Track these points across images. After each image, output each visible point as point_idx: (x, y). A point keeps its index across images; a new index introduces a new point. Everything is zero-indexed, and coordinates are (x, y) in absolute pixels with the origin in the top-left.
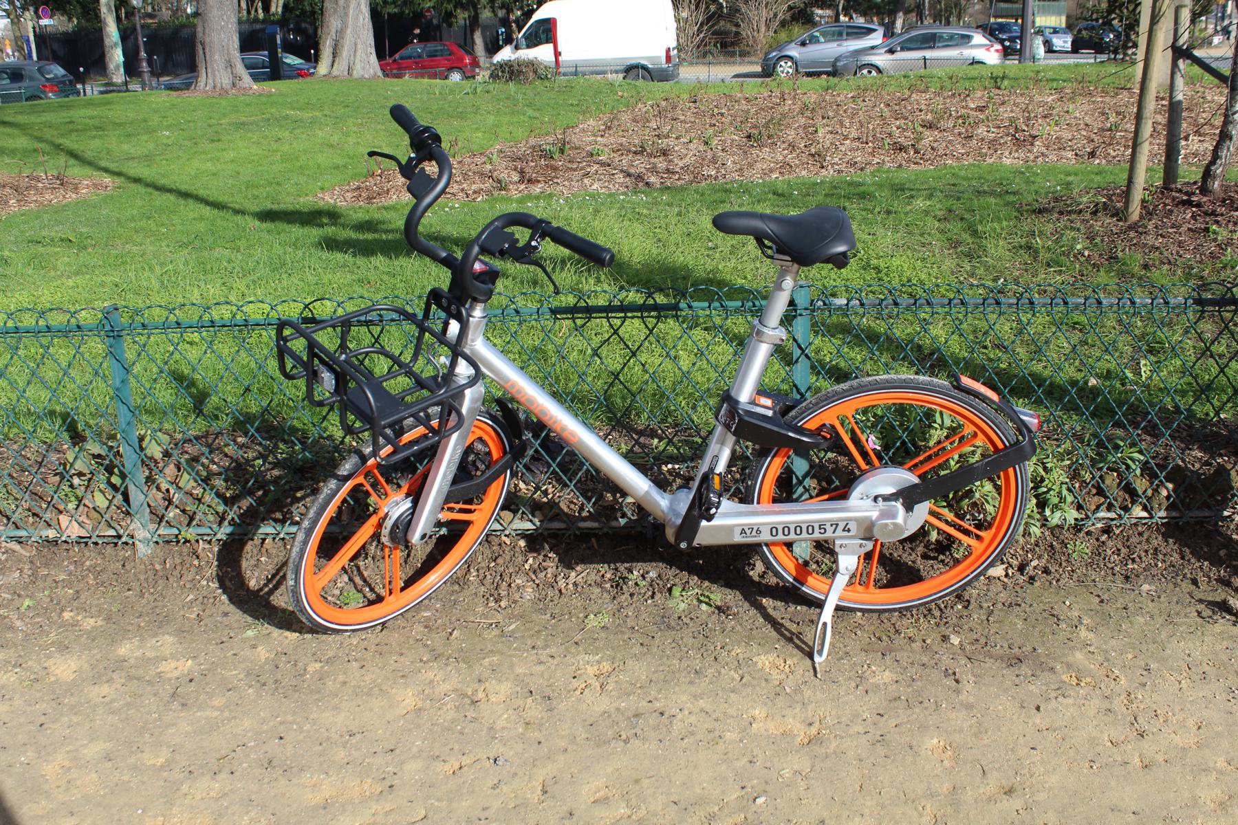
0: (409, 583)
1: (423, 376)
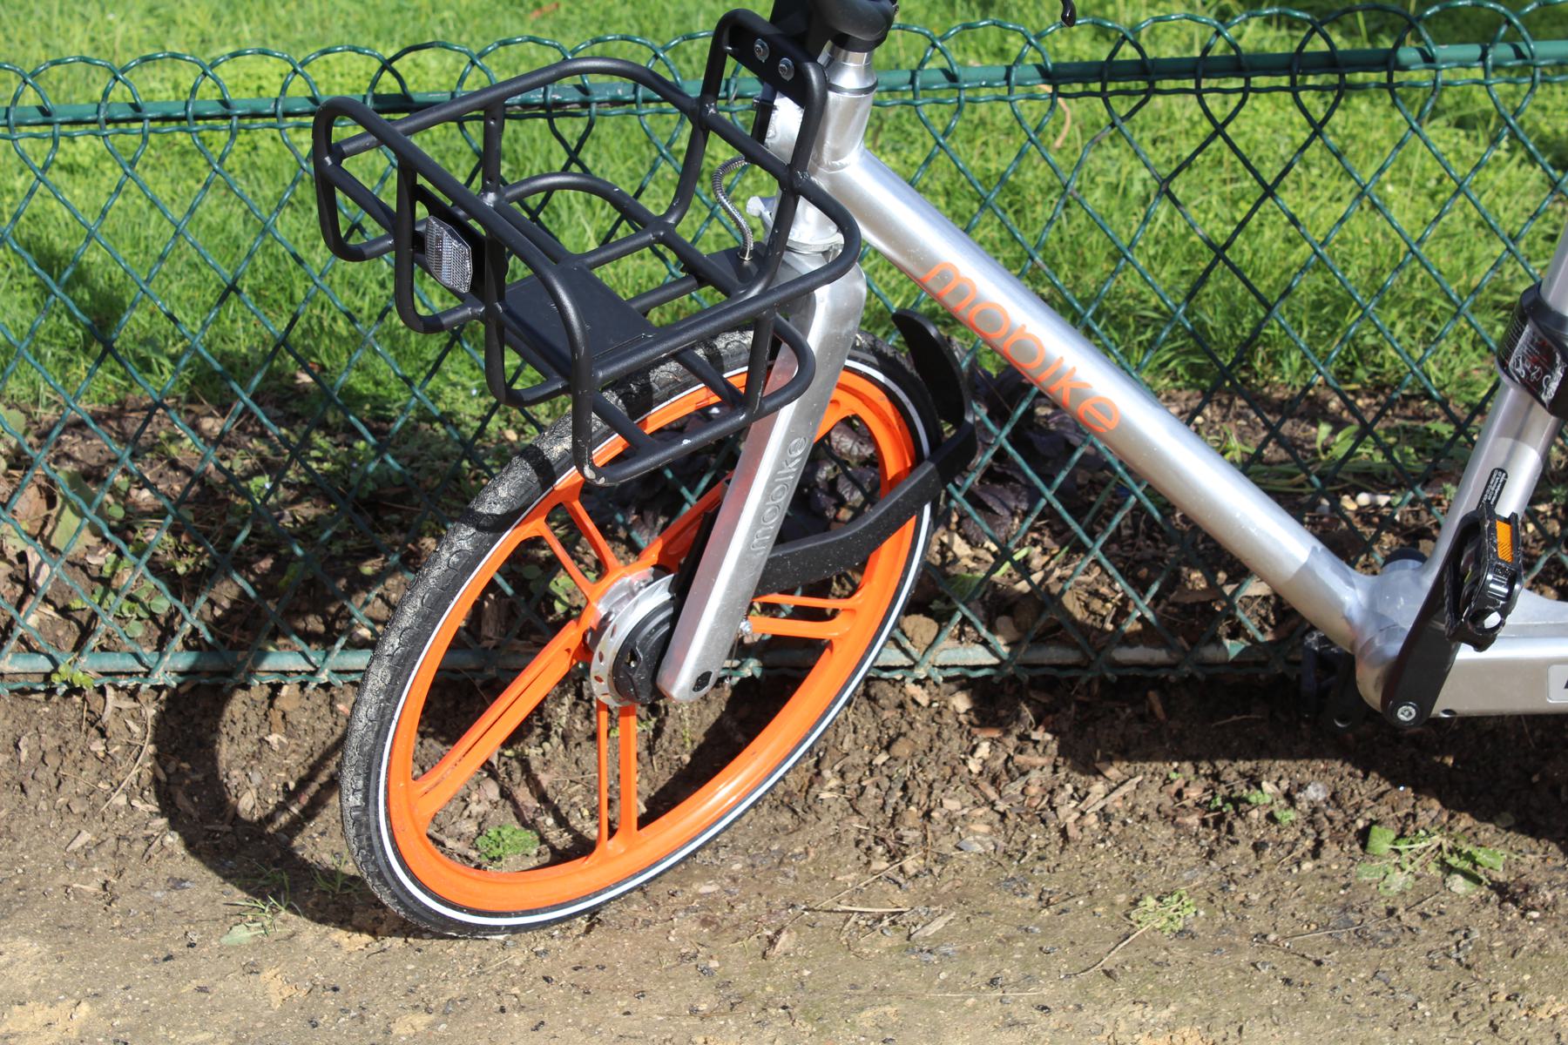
0: (660, 805)
1: (703, 250)
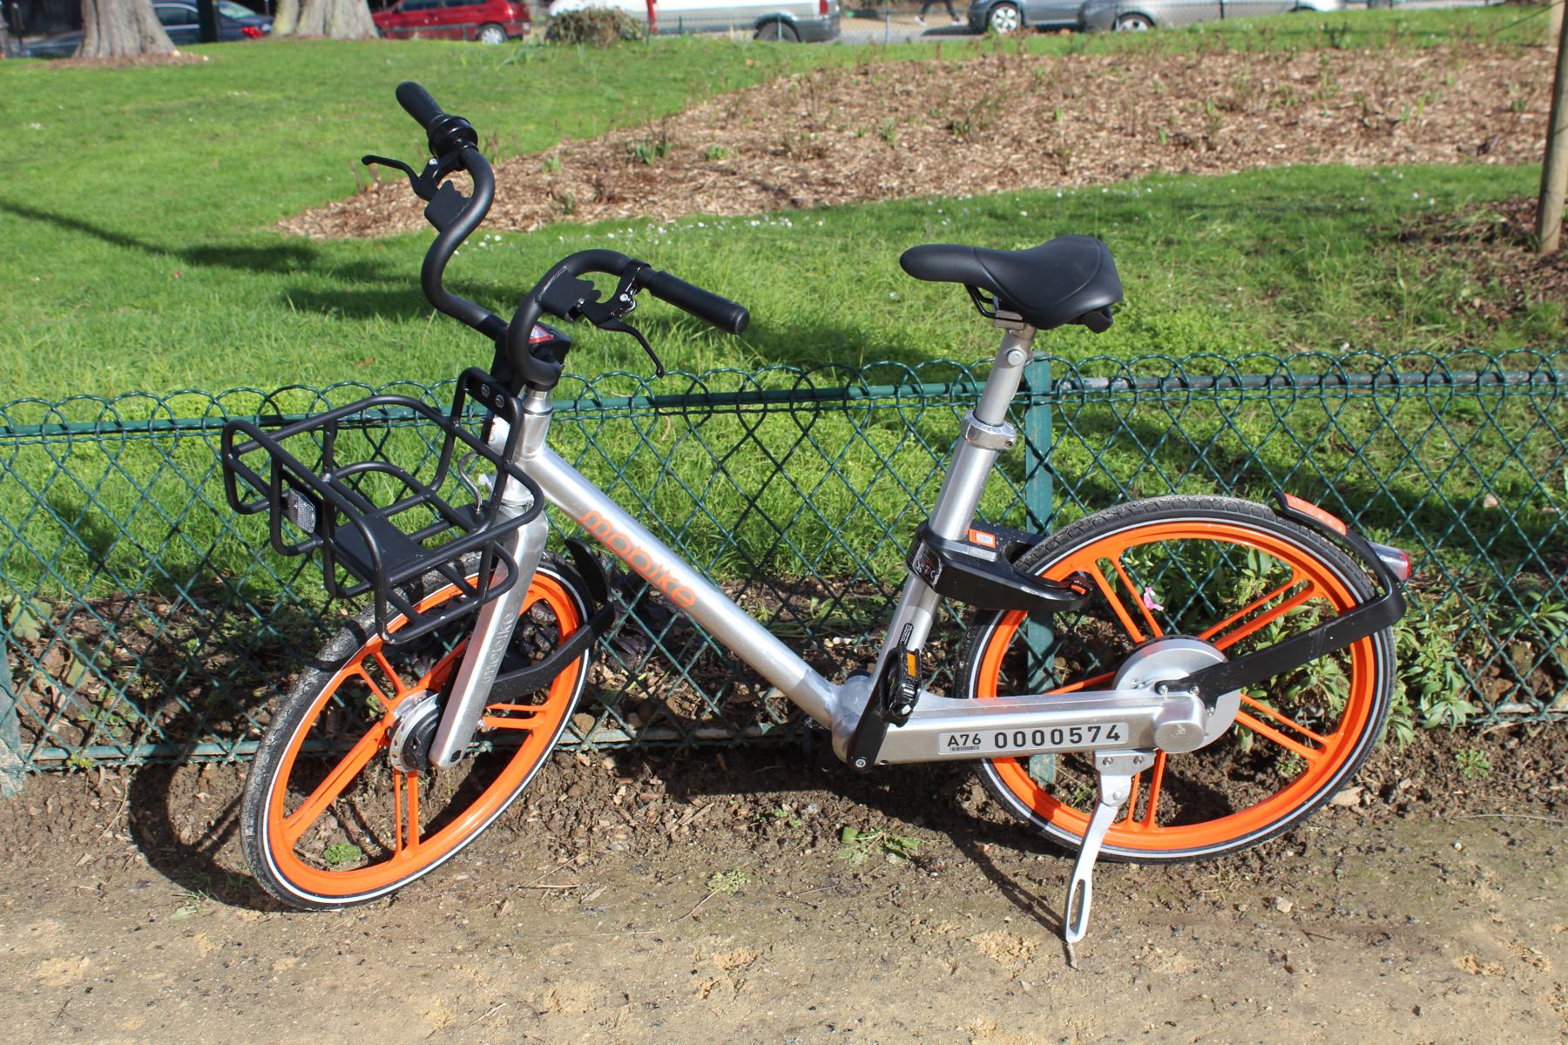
0: (433, 828)
